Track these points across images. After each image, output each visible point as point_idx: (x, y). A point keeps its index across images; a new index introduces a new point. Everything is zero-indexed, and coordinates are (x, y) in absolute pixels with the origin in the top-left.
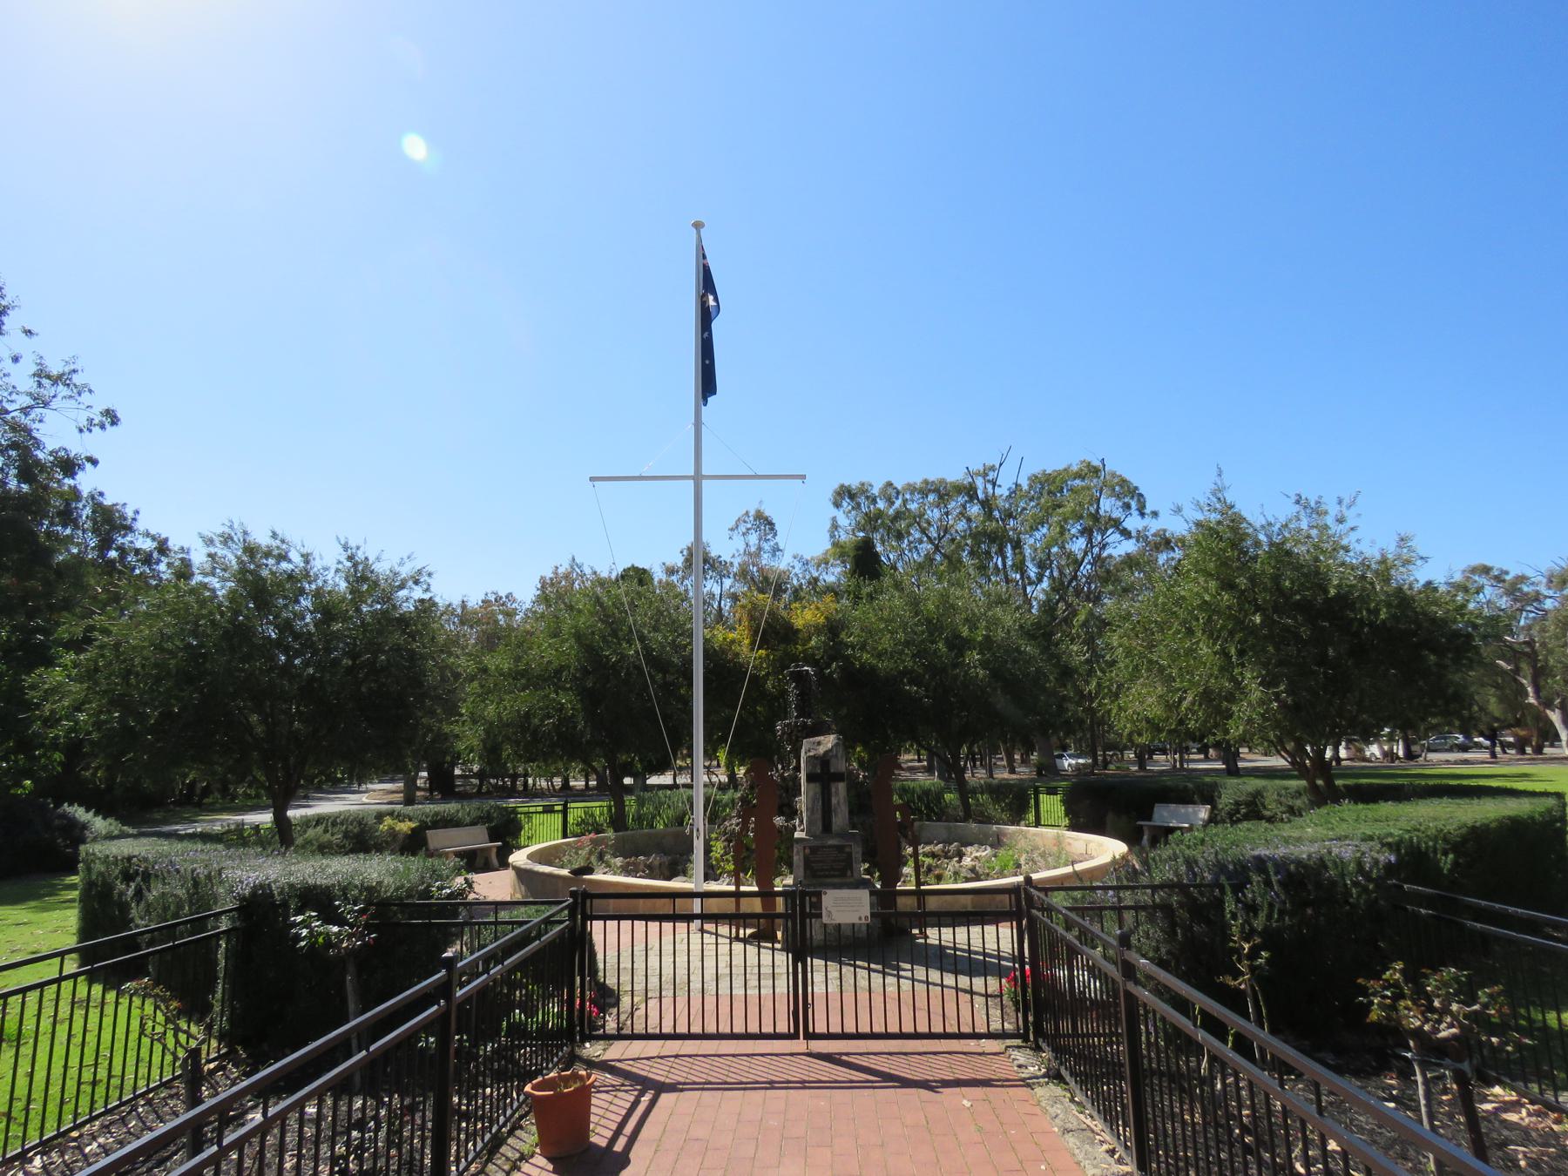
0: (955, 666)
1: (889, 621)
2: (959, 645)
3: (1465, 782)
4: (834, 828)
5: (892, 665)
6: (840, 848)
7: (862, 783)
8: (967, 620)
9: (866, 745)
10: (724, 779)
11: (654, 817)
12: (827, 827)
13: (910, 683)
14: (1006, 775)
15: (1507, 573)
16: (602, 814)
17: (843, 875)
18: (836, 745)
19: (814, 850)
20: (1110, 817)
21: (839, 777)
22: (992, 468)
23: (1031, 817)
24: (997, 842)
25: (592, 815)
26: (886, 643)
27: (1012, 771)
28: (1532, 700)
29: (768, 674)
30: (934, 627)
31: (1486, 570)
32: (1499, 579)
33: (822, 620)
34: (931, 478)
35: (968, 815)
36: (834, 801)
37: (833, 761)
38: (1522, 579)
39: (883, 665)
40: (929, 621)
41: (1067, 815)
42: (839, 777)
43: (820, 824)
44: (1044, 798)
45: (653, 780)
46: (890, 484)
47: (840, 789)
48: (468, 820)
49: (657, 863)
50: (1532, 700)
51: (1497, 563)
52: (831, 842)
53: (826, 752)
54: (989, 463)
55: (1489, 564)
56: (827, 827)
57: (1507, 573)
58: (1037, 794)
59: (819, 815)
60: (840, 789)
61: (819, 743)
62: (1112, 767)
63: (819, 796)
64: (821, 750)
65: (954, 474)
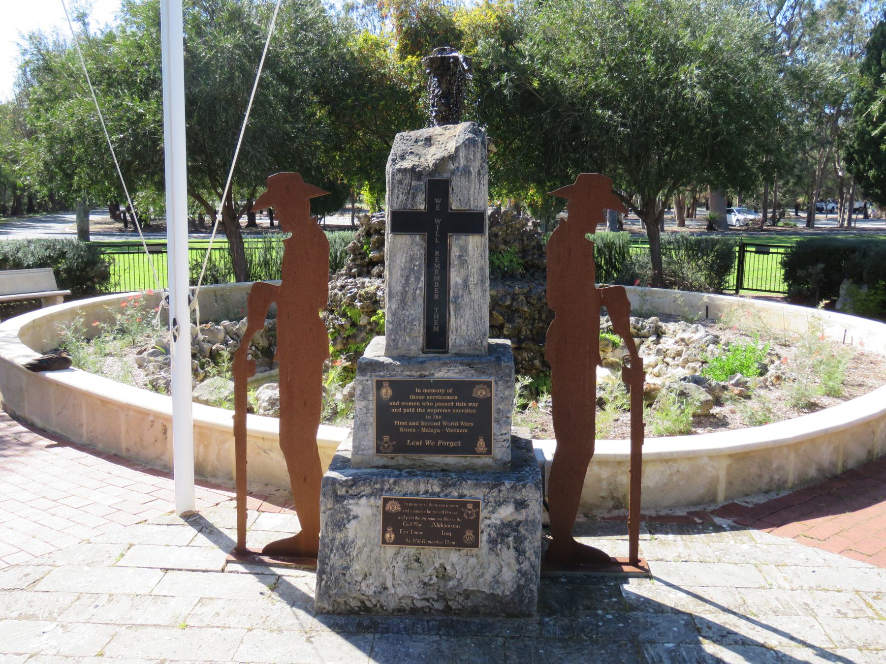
0: (664, 86)
1: (581, 23)
2: (672, 56)
4: (453, 339)
5: (580, 83)
6: (462, 389)
7: (531, 235)
8: (688, 23)
9: (540, 184)
12: (436, 339)
13: (603, 106)
14: (675, 228)
17: (468, 449)
18: (469, 144)
19: (402, 389)
20: (845, 287)
21: (471, 222)
23: (732, 279)
24: (709, 317)
26: (575, 54)
27: (682, 224)
30: (639, 35)
33: (493, 20)
35: (660, 280)
36: (455, 277)
37: (458, 183)
39: (569, 82)
40: (632, 27)
41: (786, 279)
42: (471, 222)
43: (419, 330)
44: (752, 260)
47: (471, 253)
48: (31, 260)
52: (443, 374)
53: (442, 162)
56: (436, 339)
58: (743, 252)
59: (417, 310)
60: (471, 253)
61: (428, 141)
62: (780, 224)
63: (420, 264)
64: (430, 157)
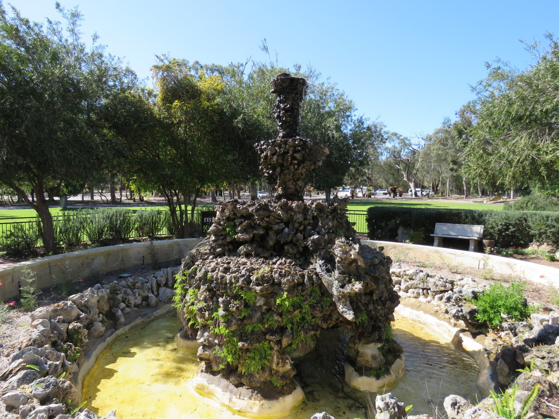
3: (415, 207)
10: (109, 198)
11: (79, 230)
15: (401, 136)
16: (31, 227)
22: (242, 65)
25: (22, 229)
28: (405, 179)
29: (180, 122)
31: (396, 134)
32: (398, 138)
34: (216, 64)
38: (406, 138)
45: (72, 198)
46: (197, 63)
49: (94, 300)
50: (405, 179)
51: (399, 132)
54: (241, 62)
55: (397, 132)
57: (401, 136)
65: (225, 65)
